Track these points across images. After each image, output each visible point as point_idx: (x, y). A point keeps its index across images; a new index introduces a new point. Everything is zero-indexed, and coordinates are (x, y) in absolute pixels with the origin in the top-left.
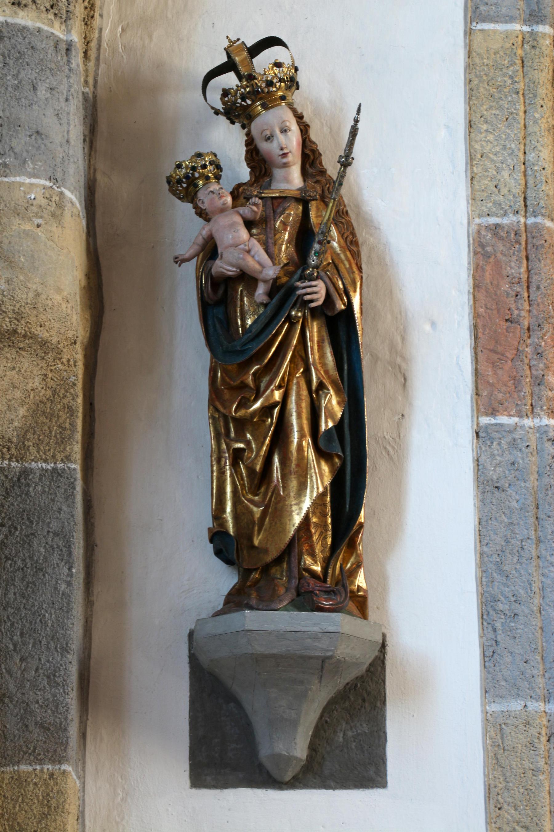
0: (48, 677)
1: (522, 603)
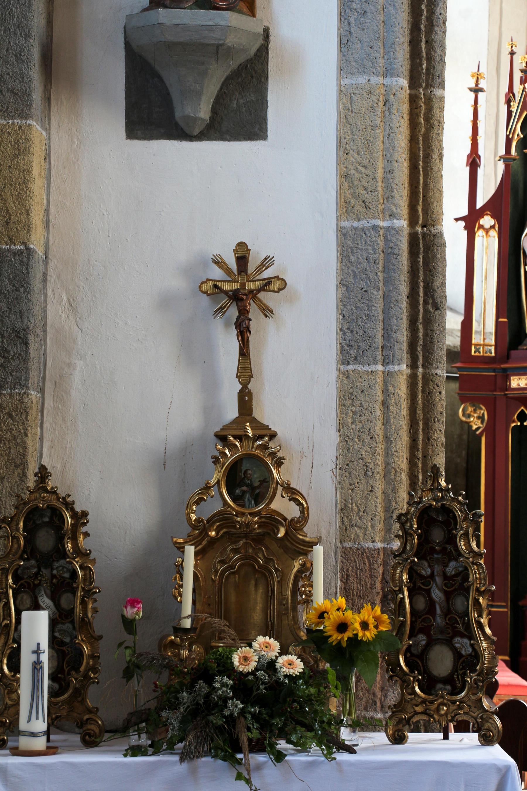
0: (16, 56)
1: (370, 3)
